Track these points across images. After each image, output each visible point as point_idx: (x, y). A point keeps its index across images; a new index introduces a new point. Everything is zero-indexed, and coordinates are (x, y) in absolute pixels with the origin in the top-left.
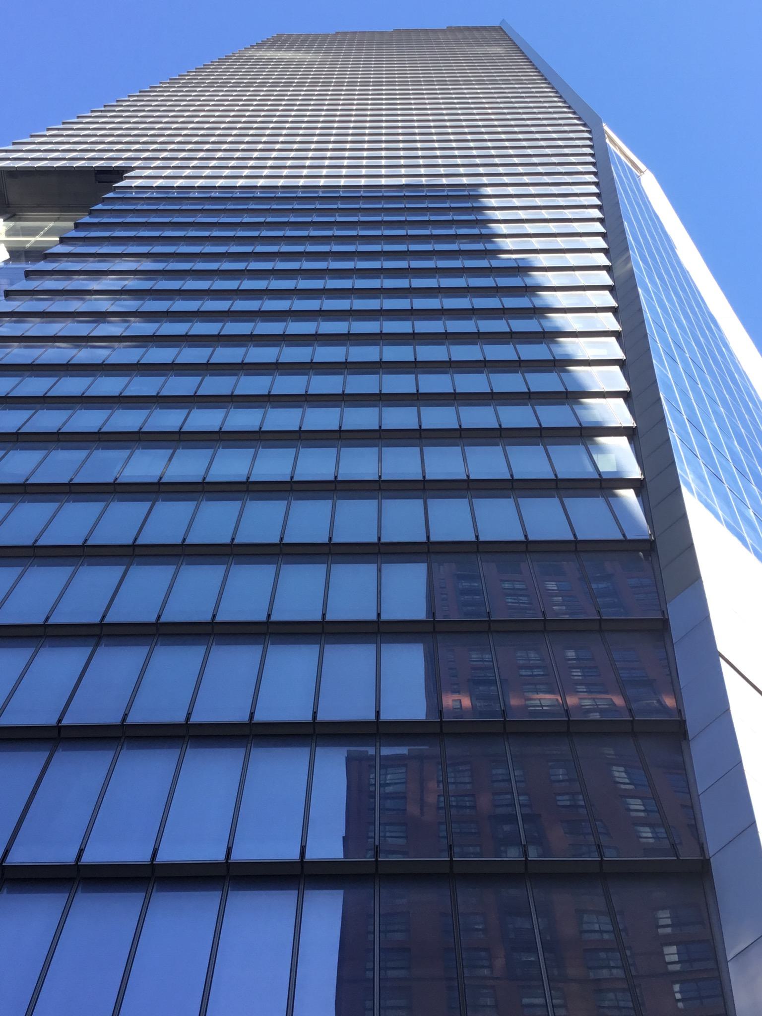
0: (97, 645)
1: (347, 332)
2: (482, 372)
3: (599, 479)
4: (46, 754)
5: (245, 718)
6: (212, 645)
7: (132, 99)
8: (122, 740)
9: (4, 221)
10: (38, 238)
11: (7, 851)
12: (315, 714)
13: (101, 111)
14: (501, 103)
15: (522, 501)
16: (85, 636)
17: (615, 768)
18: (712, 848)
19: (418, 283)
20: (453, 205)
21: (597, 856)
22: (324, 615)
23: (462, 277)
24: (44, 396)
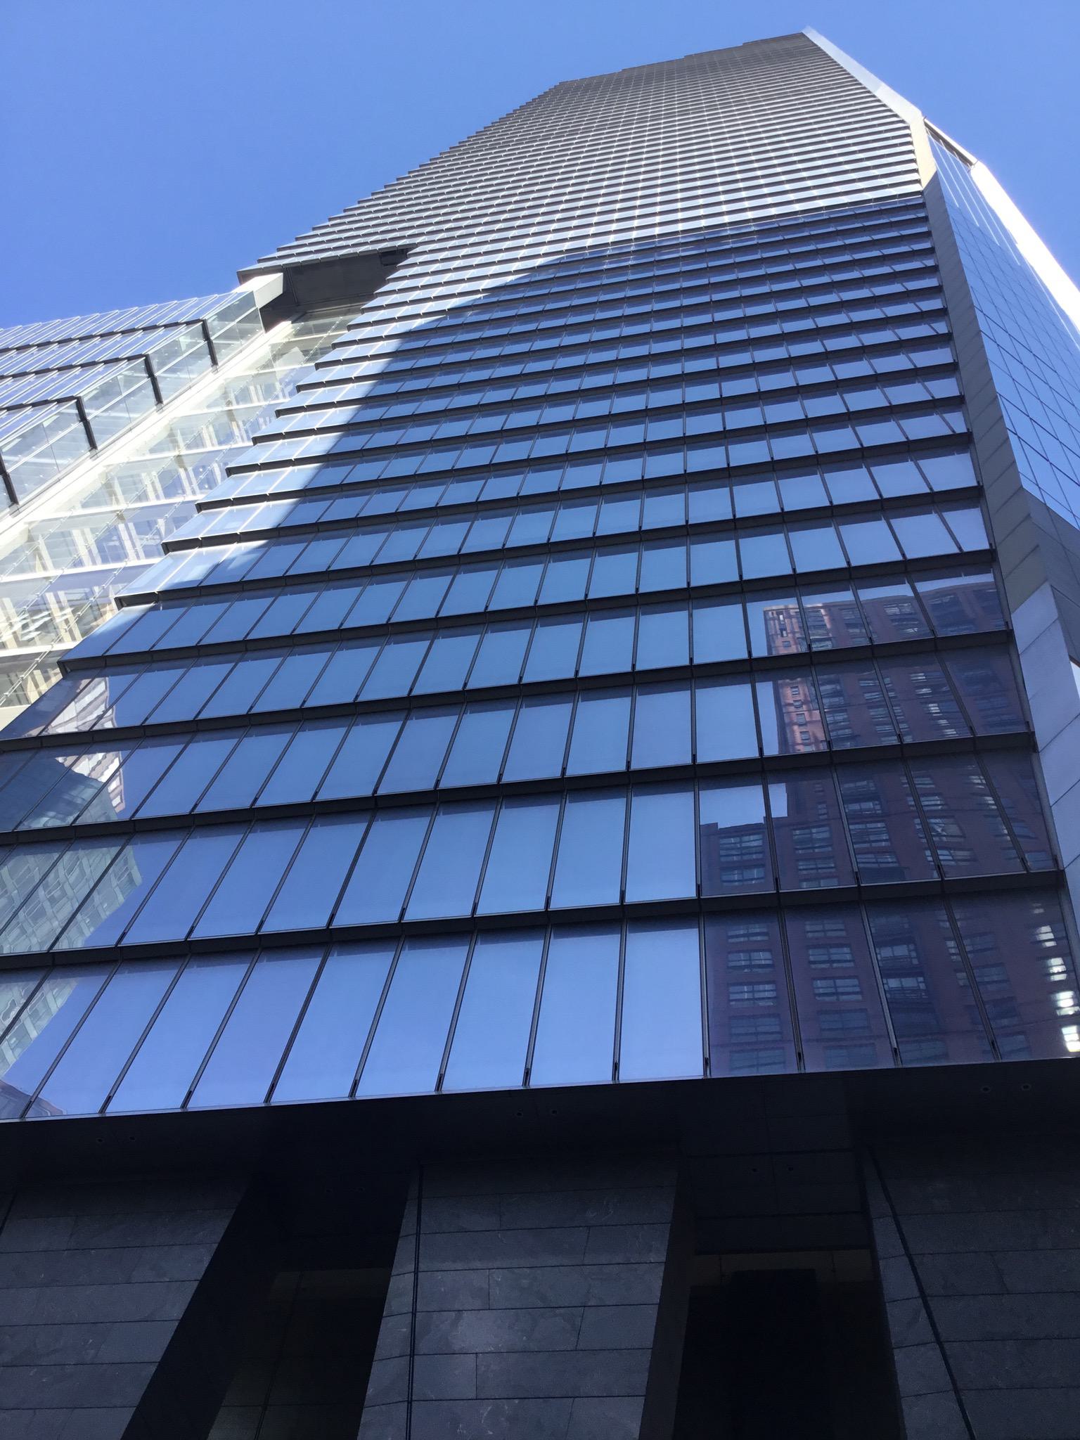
0: (406, 719)
1: (644, 408)
3: (878, 500)
4: (318, 961)
5: (557, 774)
6: (501, 808)
7: (411, 175)
9: (292, 323)
10: (325, 335)
17: (930, 705)
18: (1066, 858)
19: (724, 337)
20: (765, 255)
22: (634, 666)
23: (770, 303)
24: (340, 484)
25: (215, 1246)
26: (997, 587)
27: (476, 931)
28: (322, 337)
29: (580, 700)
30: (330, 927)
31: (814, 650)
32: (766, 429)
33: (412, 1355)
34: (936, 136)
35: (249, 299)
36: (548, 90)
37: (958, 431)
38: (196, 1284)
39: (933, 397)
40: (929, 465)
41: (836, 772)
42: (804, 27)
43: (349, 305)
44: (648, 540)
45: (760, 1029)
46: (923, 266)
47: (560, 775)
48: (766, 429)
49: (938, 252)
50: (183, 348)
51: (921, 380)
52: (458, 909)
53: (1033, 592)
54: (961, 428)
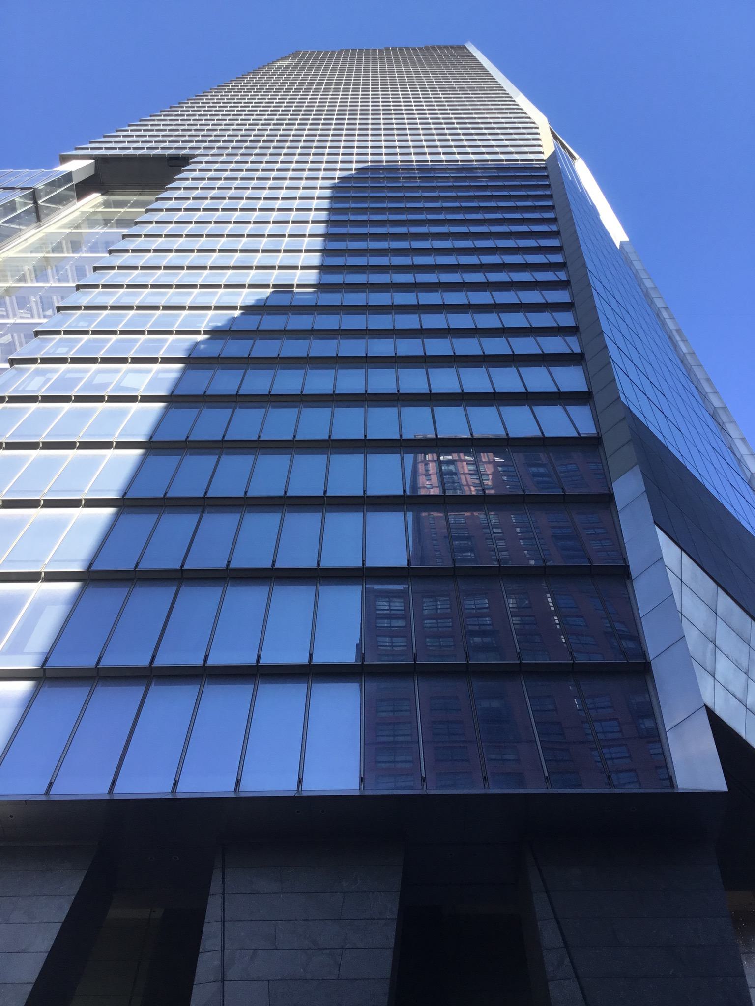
0: (203, 512)
2: (442, 313)
3: (524, 393)
4: (174, 589)
8: (135, 581)
10: (122, 210)
11: (154, 656)
12: (319, 562)
13: (168, 111)
14: (456, 105)
15: (469, 409)
16: (337, 505)
21: (465, 660)
25: (73, 898)
26: (475, 461)
27: (259, 675)
28: (120, 211)
29: (246, 512)
30: (98, 667)
31: (447, 494)
32: (449, 331)
33: (223, 981)
34: (555, 137)
35: (68, 177)
36: (295, 52)
37: (575, 351)
38: (60, 925)
39: (531, 325)
40: (496, 372)
41: (502, 580)
42: (466, 42)
43: (141, 190)
44: (403, 400)
45: (398, 759)
46: (549, 230)
47: (316, 566)
48: (449, 331)
49: (560, 222)
50: (17, 206)
51: (550, 311)
52: (248, 659)
53: (628, 471)
54: (577, 350)
